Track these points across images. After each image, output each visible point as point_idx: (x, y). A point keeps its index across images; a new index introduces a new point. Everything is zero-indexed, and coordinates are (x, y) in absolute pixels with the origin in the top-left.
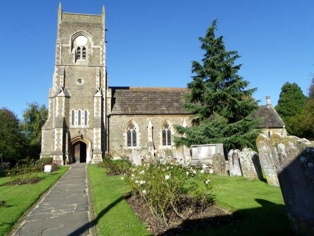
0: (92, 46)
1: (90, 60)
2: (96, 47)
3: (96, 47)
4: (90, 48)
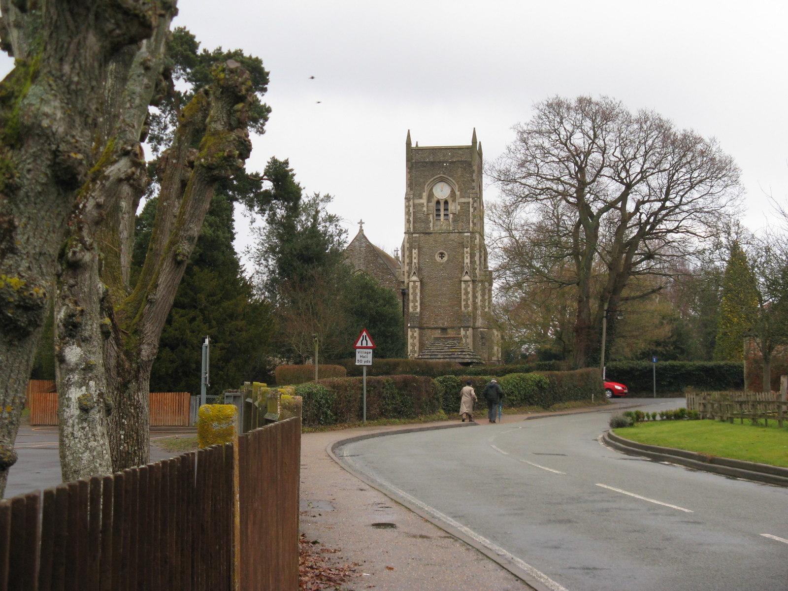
1: (454, 221)
2: (463, 200)
3: (463, 200)
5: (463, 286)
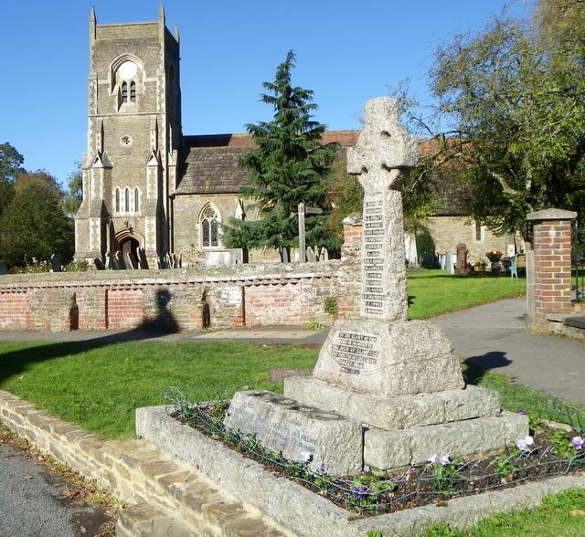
0: (144, 80)
2: (150, 80)
3: (150, 80)
4: (141, 81)
5: (149, 172)
